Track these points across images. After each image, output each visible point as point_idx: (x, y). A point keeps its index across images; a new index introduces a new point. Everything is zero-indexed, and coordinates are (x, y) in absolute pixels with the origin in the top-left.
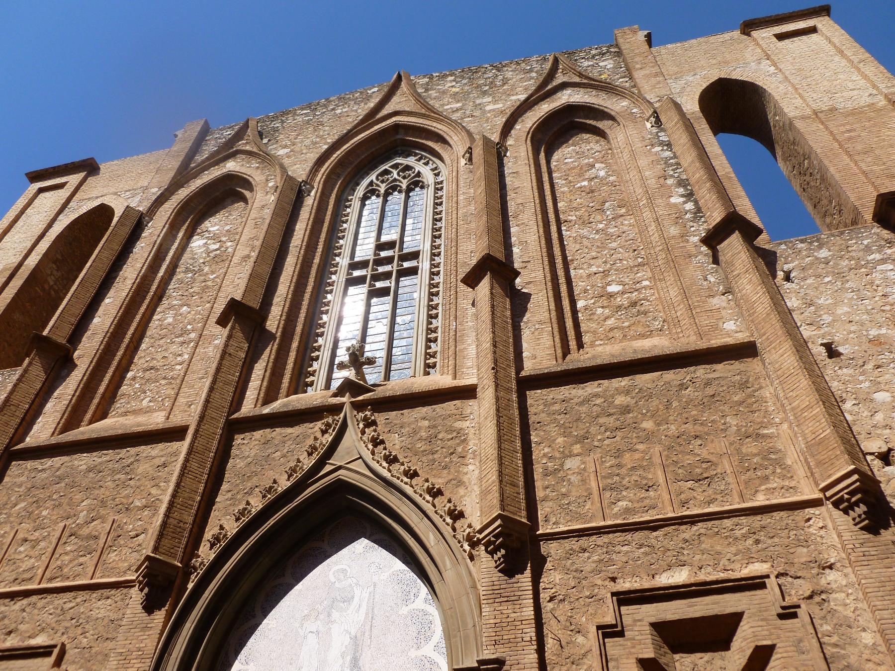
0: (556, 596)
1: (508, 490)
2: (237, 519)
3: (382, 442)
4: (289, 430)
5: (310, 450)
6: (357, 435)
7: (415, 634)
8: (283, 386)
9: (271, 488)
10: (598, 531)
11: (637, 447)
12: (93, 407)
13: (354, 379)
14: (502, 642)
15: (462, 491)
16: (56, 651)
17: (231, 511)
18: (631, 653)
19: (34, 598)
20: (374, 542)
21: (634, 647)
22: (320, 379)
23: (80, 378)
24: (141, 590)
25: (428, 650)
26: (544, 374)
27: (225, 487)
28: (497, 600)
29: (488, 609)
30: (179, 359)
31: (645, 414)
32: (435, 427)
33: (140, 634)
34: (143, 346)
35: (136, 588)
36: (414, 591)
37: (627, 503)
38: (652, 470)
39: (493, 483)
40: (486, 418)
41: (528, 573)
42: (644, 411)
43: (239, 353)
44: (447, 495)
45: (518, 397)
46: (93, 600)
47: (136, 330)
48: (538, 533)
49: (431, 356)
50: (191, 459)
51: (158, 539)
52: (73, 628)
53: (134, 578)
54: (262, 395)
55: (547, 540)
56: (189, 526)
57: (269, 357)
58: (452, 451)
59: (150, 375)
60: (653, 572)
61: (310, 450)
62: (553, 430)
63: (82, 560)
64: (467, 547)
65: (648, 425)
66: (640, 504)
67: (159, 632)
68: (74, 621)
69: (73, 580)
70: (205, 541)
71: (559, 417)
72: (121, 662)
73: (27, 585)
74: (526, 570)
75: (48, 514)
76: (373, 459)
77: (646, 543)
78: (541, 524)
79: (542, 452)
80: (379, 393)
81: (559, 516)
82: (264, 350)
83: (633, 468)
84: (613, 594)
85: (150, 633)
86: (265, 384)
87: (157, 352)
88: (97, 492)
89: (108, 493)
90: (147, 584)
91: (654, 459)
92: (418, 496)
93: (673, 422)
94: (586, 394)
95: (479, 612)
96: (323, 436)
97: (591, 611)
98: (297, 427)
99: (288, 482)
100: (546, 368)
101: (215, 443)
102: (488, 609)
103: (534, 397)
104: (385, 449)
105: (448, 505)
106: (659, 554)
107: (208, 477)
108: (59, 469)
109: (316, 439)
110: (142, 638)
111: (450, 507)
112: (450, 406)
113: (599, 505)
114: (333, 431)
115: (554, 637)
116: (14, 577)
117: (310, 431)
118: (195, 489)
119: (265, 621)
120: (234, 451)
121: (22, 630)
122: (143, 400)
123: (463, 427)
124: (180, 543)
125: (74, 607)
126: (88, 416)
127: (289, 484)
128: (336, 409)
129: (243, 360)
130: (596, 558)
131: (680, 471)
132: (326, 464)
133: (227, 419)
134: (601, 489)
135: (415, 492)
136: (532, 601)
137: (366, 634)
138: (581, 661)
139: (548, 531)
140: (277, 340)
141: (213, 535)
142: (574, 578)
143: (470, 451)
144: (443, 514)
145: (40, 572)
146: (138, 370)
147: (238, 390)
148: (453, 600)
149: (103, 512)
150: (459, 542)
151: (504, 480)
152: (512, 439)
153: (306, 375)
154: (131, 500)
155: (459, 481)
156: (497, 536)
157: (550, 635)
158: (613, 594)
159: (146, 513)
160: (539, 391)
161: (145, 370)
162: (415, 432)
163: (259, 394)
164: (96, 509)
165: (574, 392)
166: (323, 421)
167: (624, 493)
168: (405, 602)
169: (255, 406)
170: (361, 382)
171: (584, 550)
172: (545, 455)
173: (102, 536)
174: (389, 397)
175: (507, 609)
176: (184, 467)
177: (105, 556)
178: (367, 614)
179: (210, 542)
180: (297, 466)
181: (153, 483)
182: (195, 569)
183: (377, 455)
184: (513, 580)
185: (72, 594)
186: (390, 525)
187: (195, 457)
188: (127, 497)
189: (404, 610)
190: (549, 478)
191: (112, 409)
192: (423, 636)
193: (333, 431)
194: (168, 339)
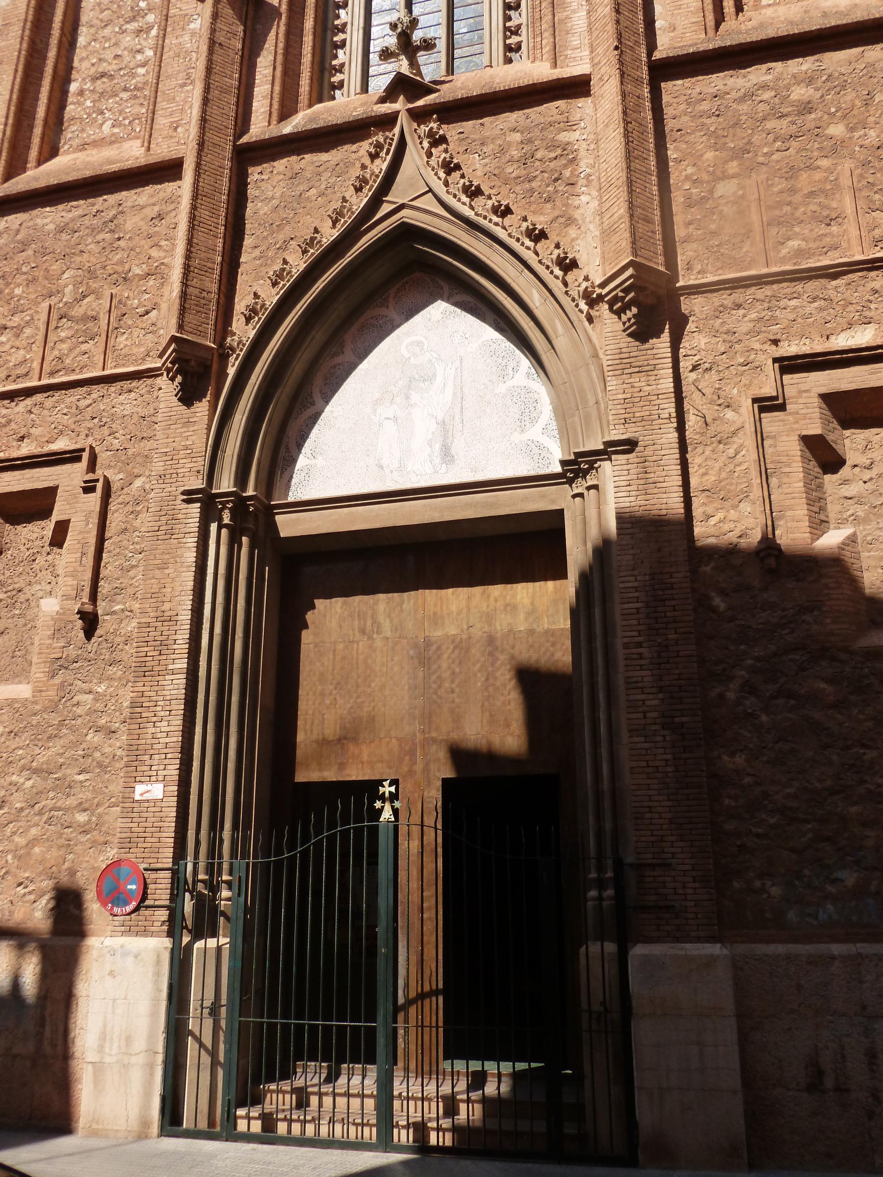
0: (700, 365)
1: (641, 227)
2: (275, 284)
3: (458, 167)
4: (324, 157)
5: (357, 184)
6: (422, 159)
7: (517, 416)
8: (301, 90)
9: (313, 239)
10: (760, 281)
11: (820, 163)
12: (36, 141)
13: (407, 73)
14: (633, 420)
15: (572, 232)
16: (85, 456)
17: (263, 273)
18: (793, 430)
19: (38, 397)
20: (456, 304)
21: (797, 422)
22: (352, 76)
23: (7, 97)
24: (172, 379)
25: (535, 433)
26: (688, 54)
27: (248, 242)
28: (626, 371)
29: (615, 383)
30: (139, 57)
31: (834, 114)
32: (530, 141)
33: (183, 430)
34: (81, 41)
35: (165, 376)
36: (512, 364)
37: (800, 242)
38: (837, 196)
39: (620, 219)
40: (607, 126)
41: (666, 336)
42: (833, 110)
43: (233, 42)
44: (553, 237)
45: (651, 92)
46: (113, 395)
47: (65, 14)
48: (677, 285)
49: (512, 33)
50: (198, 205)
51: (180, 314)
52: (98, 429)
53: (159, 365)
54: (276, 106)
55: (689, 294)
56: (214, 296)
57: (276, 46)
58: (556, 175)
59: (104, 86)
60: (828, 333)
61: (357, 184)
62: (699, 140)
63: (84, 347)
64: (583, 306)
65: (837, 130)
66: (818, 244)
67: (206, 426)
68: (96, 421)
69: (81, 372)
70: (237, 315)
71: (708, 121)
72: (168, 463)
73: (25, 382)
74: (663, 332)
75: (23, 291)
76: (448, 192)
77: (821, 296)
78: (681, 272)
79: (684, 173)
80: (445, 94)
81: (706, 261)
82: (266, 35)
83: (812, 194)
84: (775, 360)
85: (195, 428)
86: (277, 88)
87: (104, 48)
88: (78, 259)
89: (93, 259)
90: (178, 372)
91: (841, 180)
92: (513, 241)
93: (873, 126)
94: (748, 85)
95: (602, 386)
96: (372, 162)
97: (744, 381)
98: (334, 152)
99: (335, 231)
100: (690, 46)
101: (226, 180)
102: (615, 383)
103: (672, 89)
104: (463, 176)
105: (556, 252)
106: (837, 309)
107: (225, 229)
108: (18, 232)
109: (364, 167)
110: (186, 434)
111: (559, 255)
112: (551, 109)
113: (762, 245)
114: (387, 153)
115: (696, 412)
116: (5, 373)
117: (354, 156)
118: (213, 247)
119: (328, 409)
120: (251, 192)
121: (36, 434)
122: (102, 124)
123: (571, 140)
124: (208, 318)
125: (91, 405)
126: (33, 153)
127: (335, 233)
128: (387, 121)
129: (240, 53)
130: (753, 316)
131: (877, 196)
132: (383, 202)
133: (234, 146)
134: (765, 224)
135: (510, 235)
136: (671, 370)
137: (457, 417)
138: (730, 440)
139: (692, 282)
140: (283, 18)
141: (248, 306)
142: (724, 341)
143: (582, 176)
144: (550, 264)
145: (36, 365)
146: (84, 79)
147: (241, 101)
148: (567, 372)
149: (94, 285)
150: (573, 300)
151: (636, 214)
152: (644, 155)
153: (330, 72)
154: (127, 266)
155: (569, 219)
156: (626, 291)
157: (691, 412)
158: (775, 360)
159: (151, 283)
160: (680, 82)
161: (94, 79)
162: (502, 150)
163: (271, 105)
164: (85, 282)
165: (731, 82)
166: (370, 141)
167: (797, 229)
168: (501, 378)
169: (269, 123)
170: (418, 78)
171: (739, 306)
172: (687, 178)
173: (101, 315)
174: (462, 99)
175: (639, 381)
176: (192, 218)
177: (113, 340)
178: (454, 394)
179: (245, 315)
180: (344, 207)
181: (150, 242)
182: (233, 350)
183: (452, 186)
184: (647, 346)
185: (85, 389)
186: (478, 282)
187: (202, 202)
188: (121, 262)
189: (502, 388)
190: (693, 210)
191: (62, 141)
192: (527, 417)
193: (387, 153)
194: (115, 25)
